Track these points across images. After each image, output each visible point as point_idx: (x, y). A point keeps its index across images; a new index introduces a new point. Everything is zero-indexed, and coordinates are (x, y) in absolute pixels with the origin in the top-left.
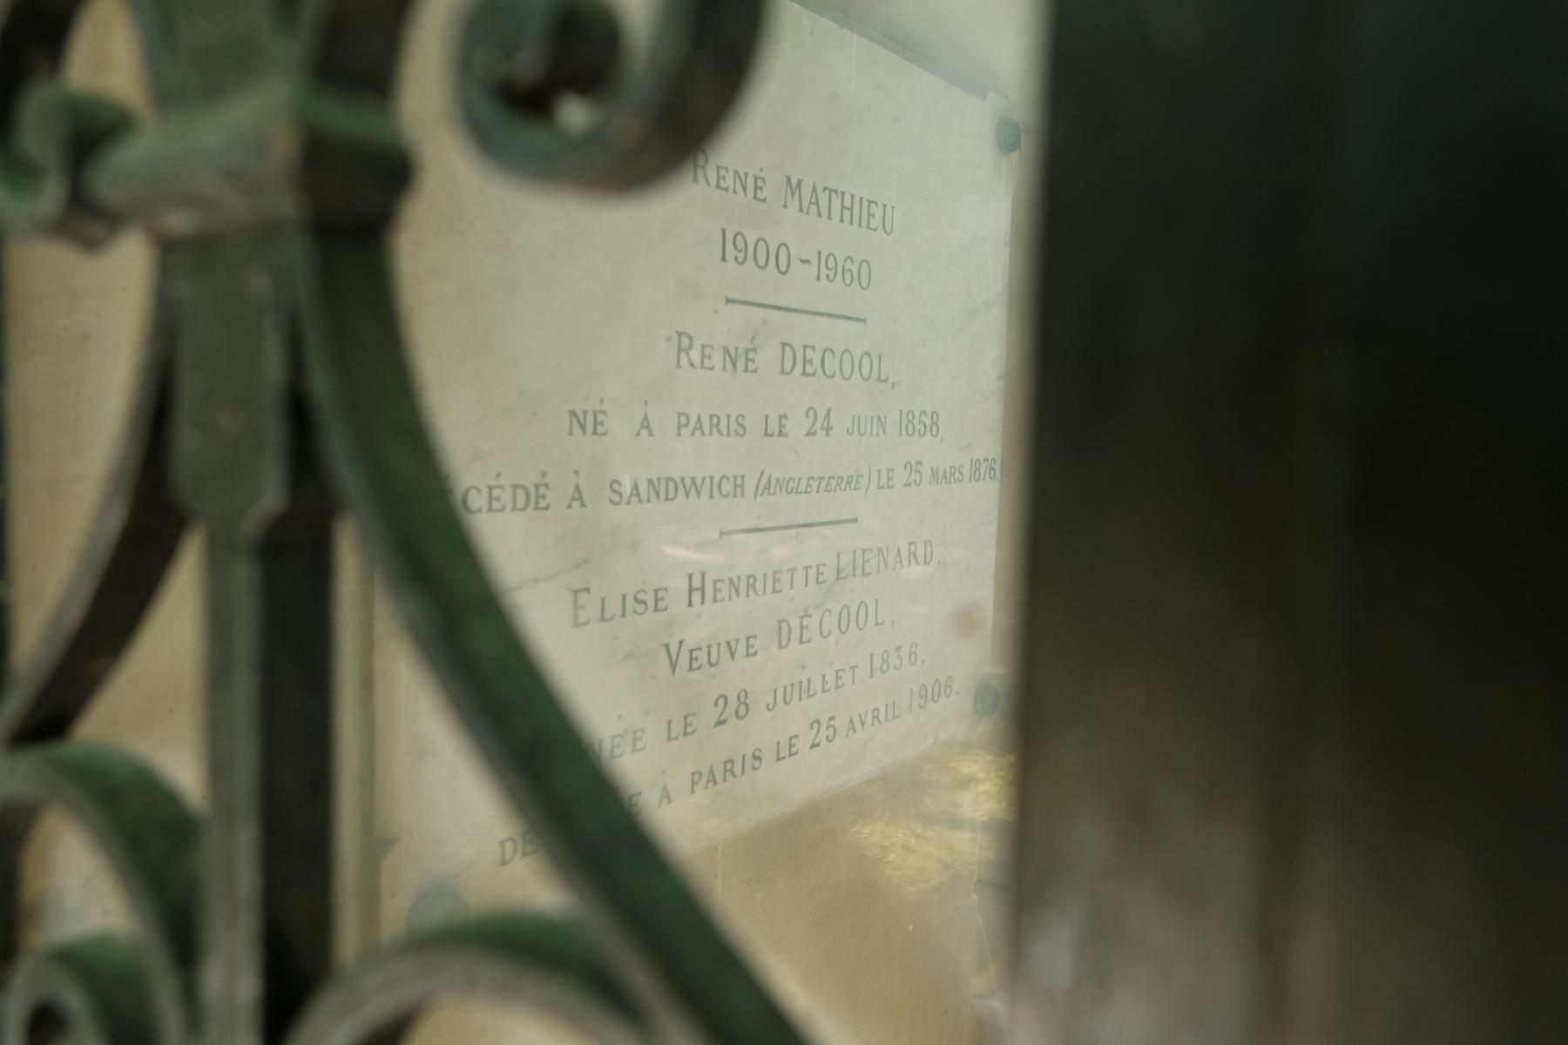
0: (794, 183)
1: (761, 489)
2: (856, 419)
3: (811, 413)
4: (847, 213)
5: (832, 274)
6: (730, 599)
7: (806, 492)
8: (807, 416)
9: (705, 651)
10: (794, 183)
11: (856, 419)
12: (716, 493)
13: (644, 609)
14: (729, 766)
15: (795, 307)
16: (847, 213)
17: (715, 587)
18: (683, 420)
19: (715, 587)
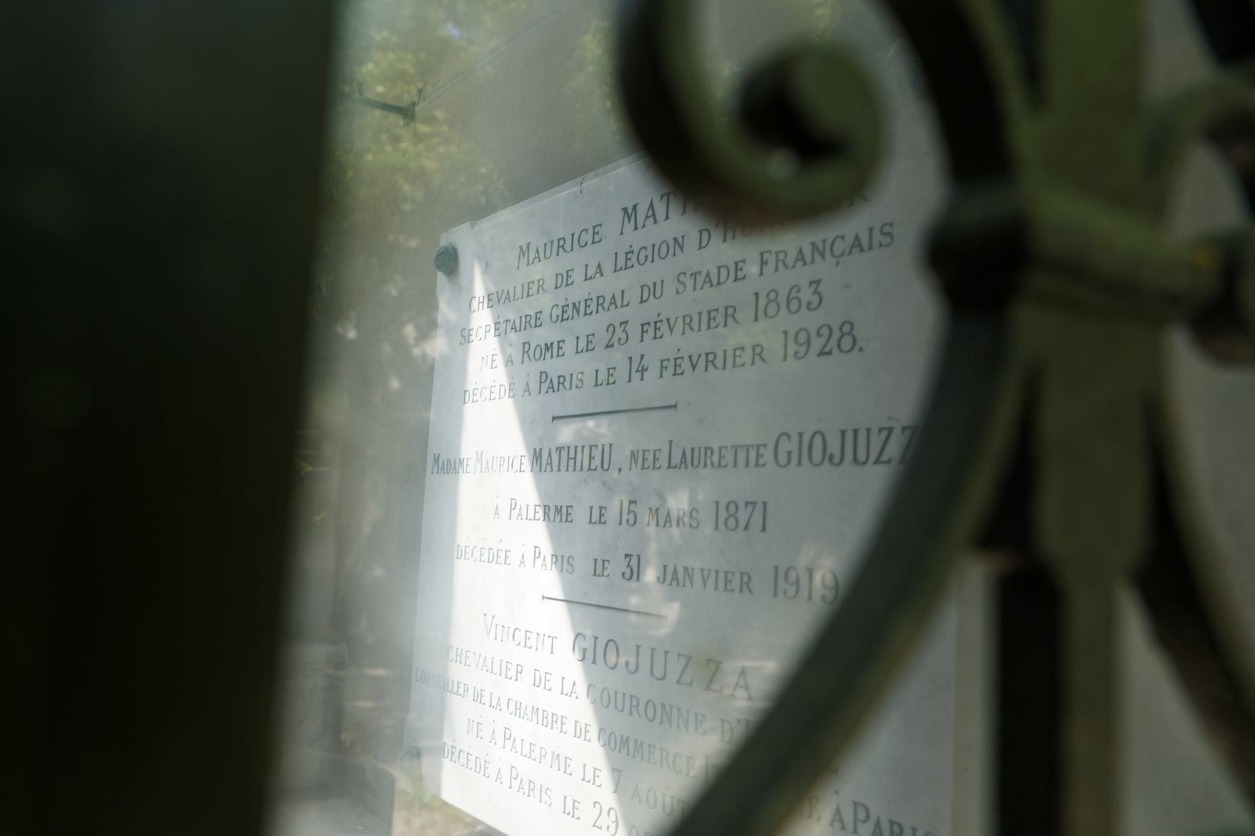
0: (639, 743)
1: (483, 468)
2: (849, 436)
3: (611, 329)
4: (572, 462)
5: (803, 349)
6: (597, 312)
7: (626, 268)
8: (607, 330)
9: (495, 295)
10: (639, 743)
11: (849, 436)
12: (761, 314)
13: (733, 311)
14: (758, 350)
15: (590, 607)
16: (572, 455)
17: (762, 258)
18: (862, 815)
19: (762, 258)
